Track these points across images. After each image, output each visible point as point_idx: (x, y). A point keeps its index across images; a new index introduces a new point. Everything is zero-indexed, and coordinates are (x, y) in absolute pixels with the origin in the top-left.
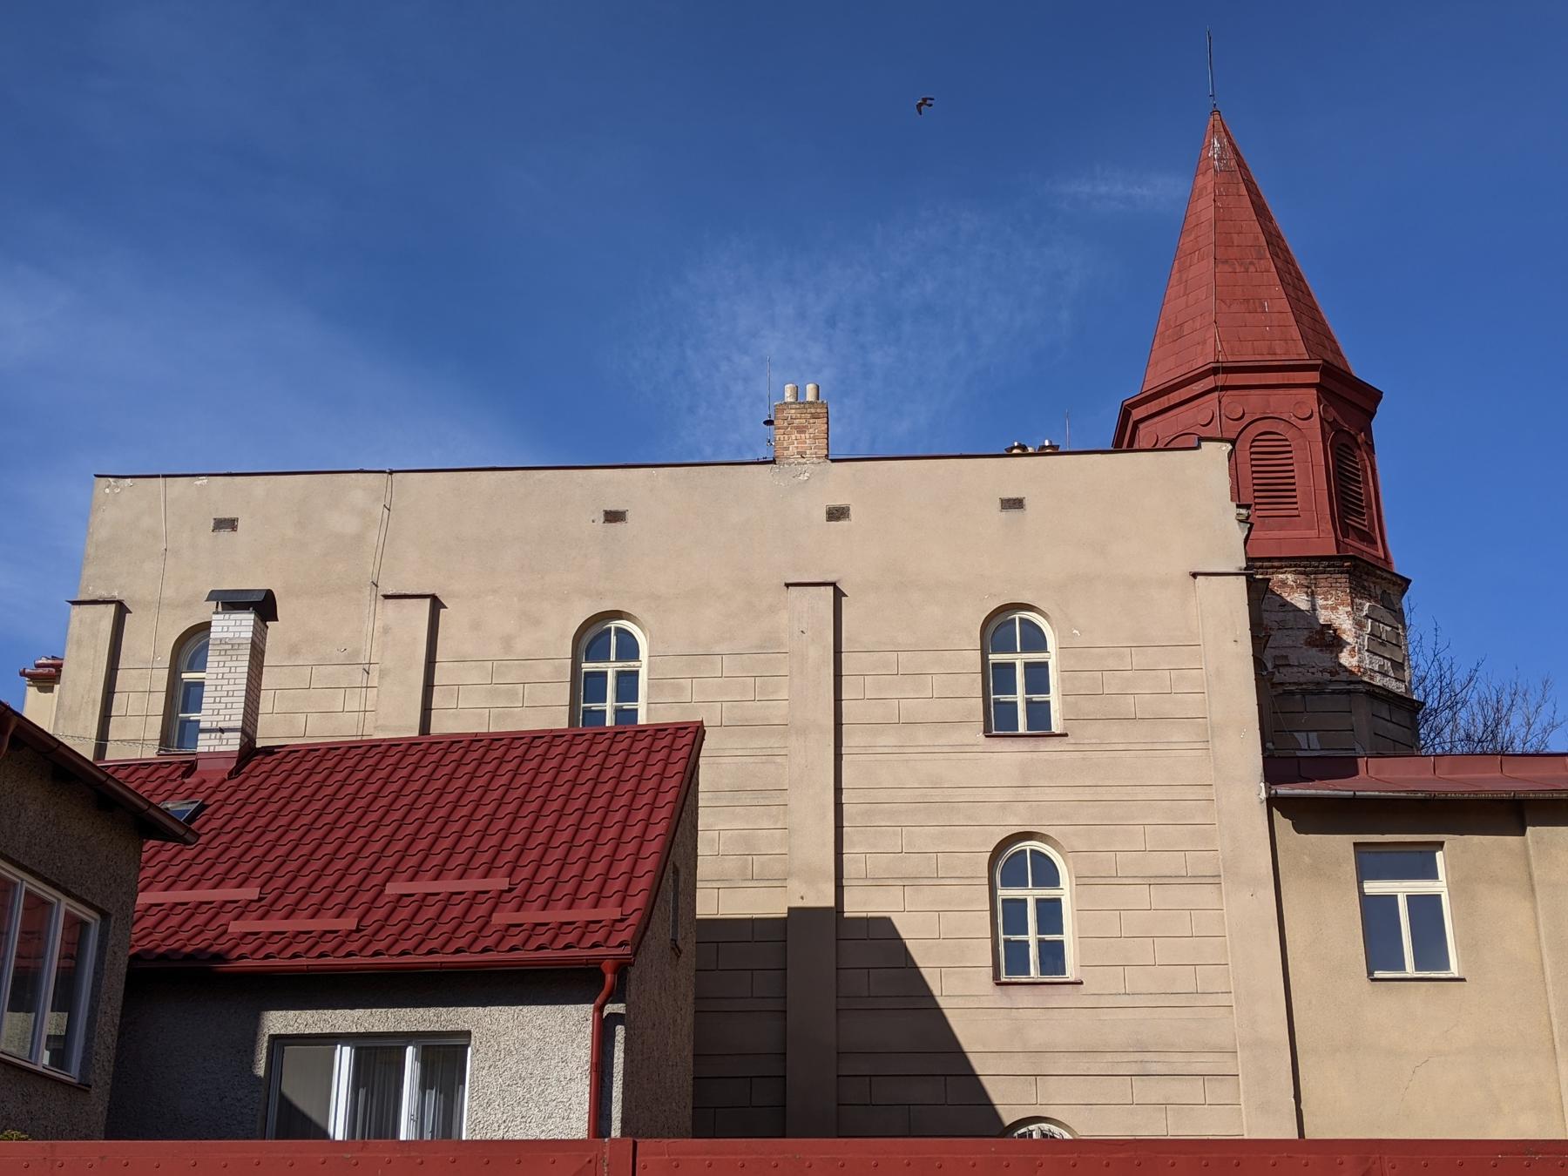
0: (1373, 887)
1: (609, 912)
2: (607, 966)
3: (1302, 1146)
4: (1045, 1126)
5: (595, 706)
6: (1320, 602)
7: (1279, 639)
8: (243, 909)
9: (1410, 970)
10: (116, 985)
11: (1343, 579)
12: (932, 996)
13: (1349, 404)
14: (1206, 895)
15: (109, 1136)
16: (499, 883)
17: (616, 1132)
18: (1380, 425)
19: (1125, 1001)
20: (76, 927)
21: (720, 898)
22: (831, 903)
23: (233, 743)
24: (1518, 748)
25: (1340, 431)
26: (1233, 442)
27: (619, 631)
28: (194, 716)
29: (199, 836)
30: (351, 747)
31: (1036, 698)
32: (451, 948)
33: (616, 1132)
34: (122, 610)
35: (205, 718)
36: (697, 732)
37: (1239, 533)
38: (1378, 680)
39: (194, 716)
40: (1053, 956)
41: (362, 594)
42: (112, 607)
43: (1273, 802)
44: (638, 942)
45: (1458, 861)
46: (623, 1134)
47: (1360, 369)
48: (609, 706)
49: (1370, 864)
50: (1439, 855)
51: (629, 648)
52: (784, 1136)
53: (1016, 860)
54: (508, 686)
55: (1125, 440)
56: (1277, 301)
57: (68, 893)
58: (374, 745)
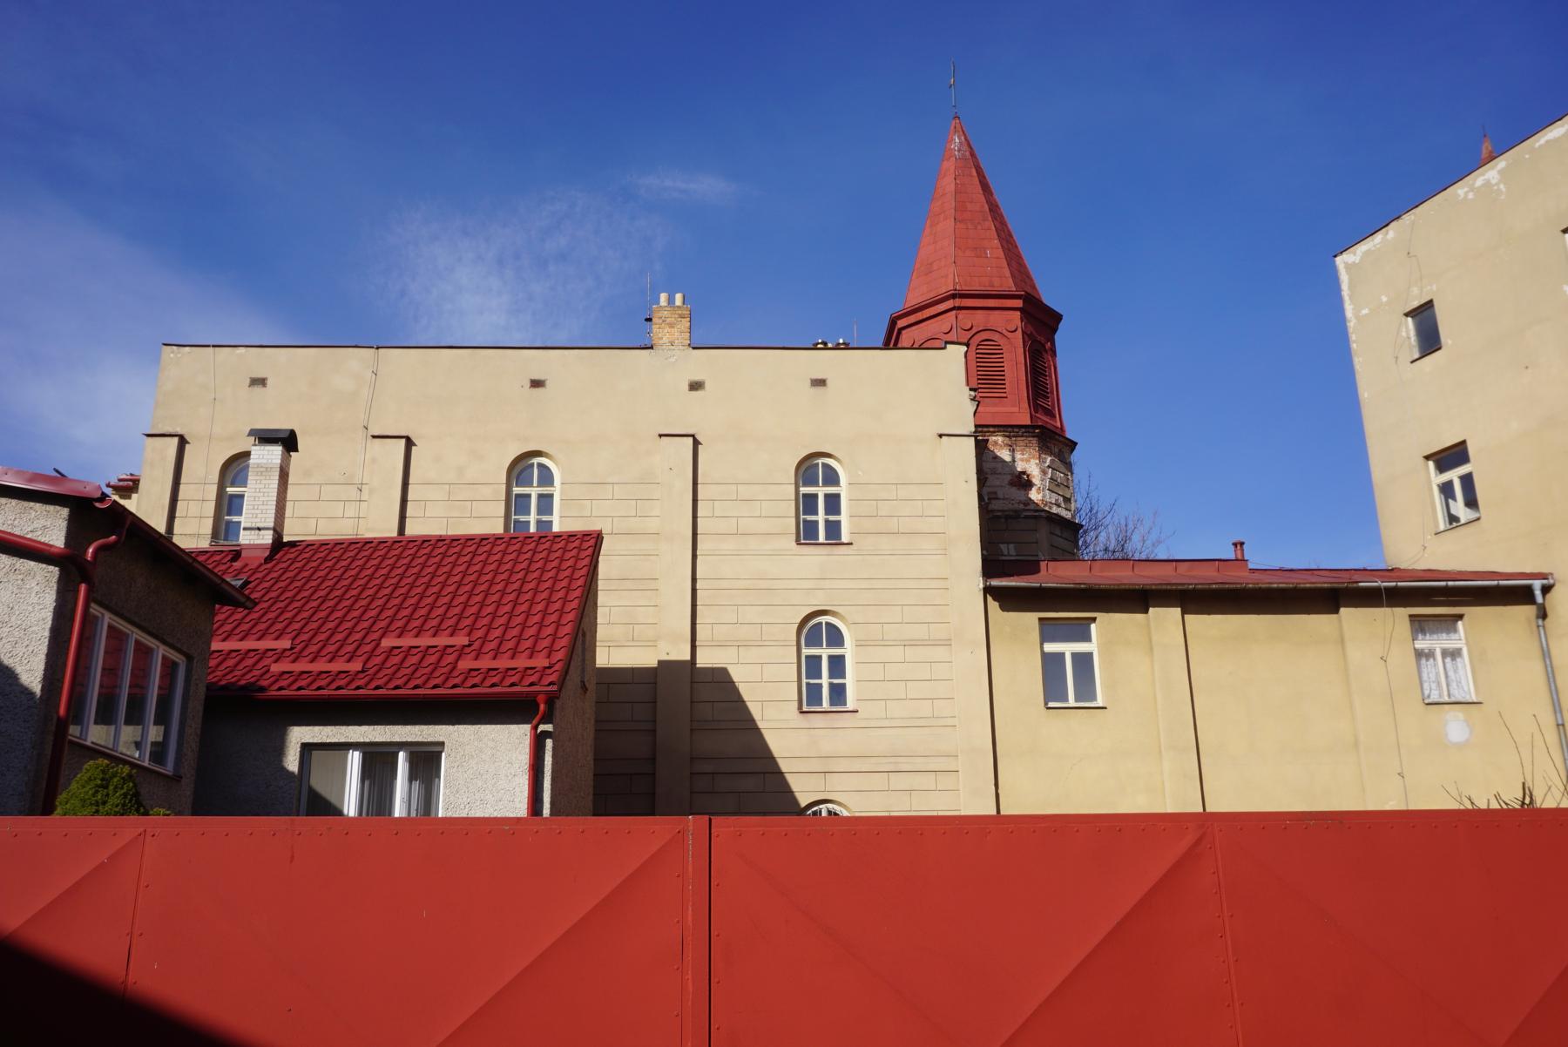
0: (1050, 647)
1: (540, 662)
2: (541, 698)
3: (999, 818)
4: (830, 806)
5: (522, 518)
6: (1018, 456)
7: (993, 481)
8: (280, 656)
9: (1072, 702)
10: (197, 706)
11: (1034, 441)
12: (753, 721)
13: (1041, 323)
14: (940, 653)
15: (195, 813)
16: (460, 640)
17: (546, 811)
18: (1063, 337)
19: (886, 723)
20: (170, 668)
21: (609, 655)
22: (688, 657)
23: (267, 538)
24: (1137, 557)
25: (1035, 341)
26: (967, 345)
27: (541, 466)
28: (235, 519)
29: (256, 604)
30: (353, 543)
31: (832, 518)
32: (411, 685)
33: (546, 811)
34: (183, 441)
35: (244, 520)
36: (598, 538)
37: (971, 407)
38: (1055, 510)
39: (235, 519)
40: (838, 693)
41: (357, 435)
42: (176, 440)
43: (987, 590)
44: (562, 682)
45: (1107, 629)
46: (552, 814)
47: (1049, 298)
48: (532, 518)
49: (1049, 631)
50: (1093, 626)
51: (546, 477)
52: (653, 814)
53: (816, 630)
54: (460, 502)
55: (892, 341)
56: (994, 250)
57: (164, 642)
58: (368, 542)
